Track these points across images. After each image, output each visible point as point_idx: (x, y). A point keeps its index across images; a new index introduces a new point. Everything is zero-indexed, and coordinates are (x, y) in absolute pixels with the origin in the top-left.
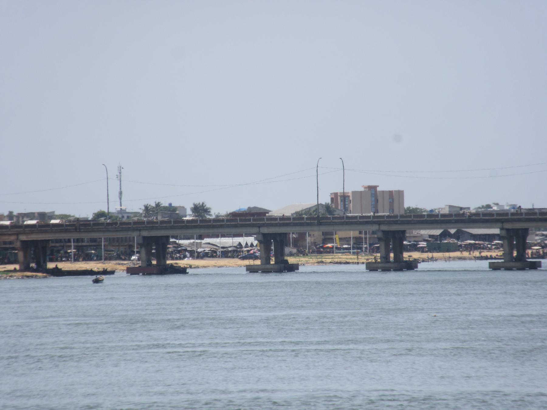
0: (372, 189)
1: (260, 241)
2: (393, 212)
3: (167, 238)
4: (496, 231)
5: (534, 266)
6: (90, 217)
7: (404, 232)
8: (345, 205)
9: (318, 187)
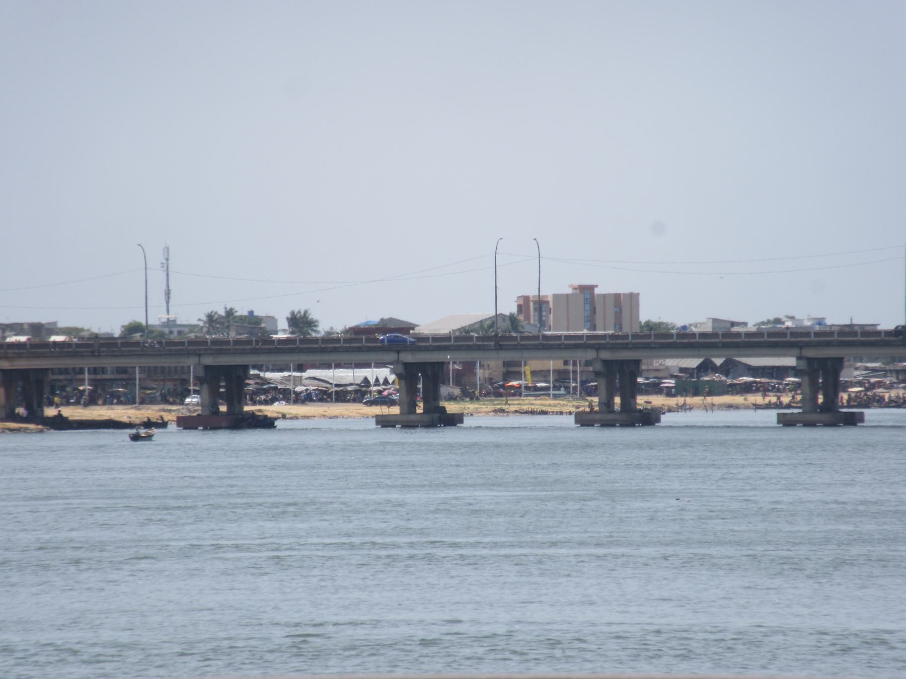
0: (587, 290)
1: (399, 376)
2: (621, 328)
3: (246, 368)
4: (790, 361)
5: (852, 420)
7: (637, 363)
8: (540, 316)
9: (496, 287)
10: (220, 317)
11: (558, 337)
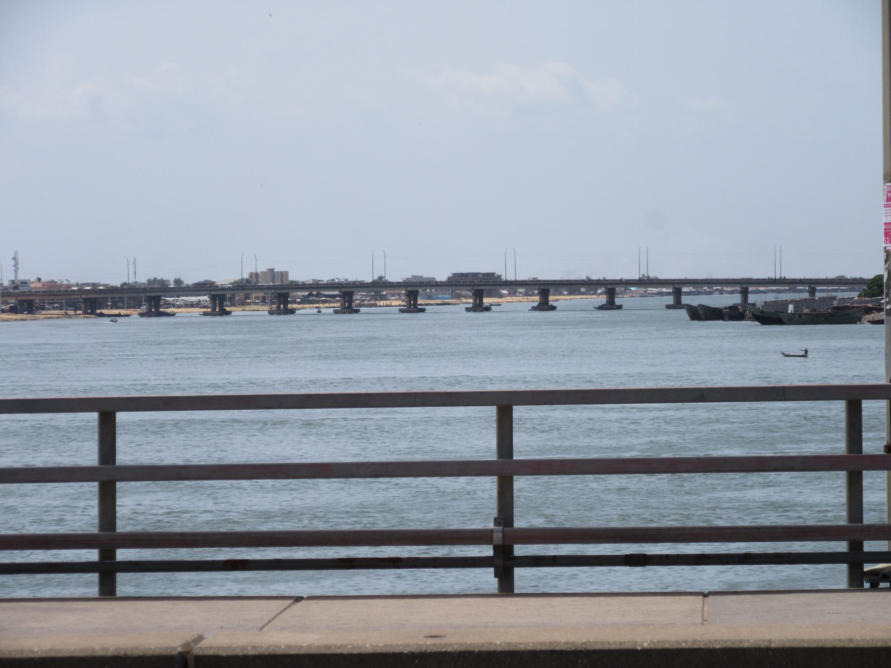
0: (272, 270)
1: (211, 299)
2: (283, 282)
3: (160, 297)
4: (337, 293)
5: (357, 311)
6: (119, 286)
7: (288, 294)
8: (257, 279)
10: (152, 280)
11: (263, 286)
